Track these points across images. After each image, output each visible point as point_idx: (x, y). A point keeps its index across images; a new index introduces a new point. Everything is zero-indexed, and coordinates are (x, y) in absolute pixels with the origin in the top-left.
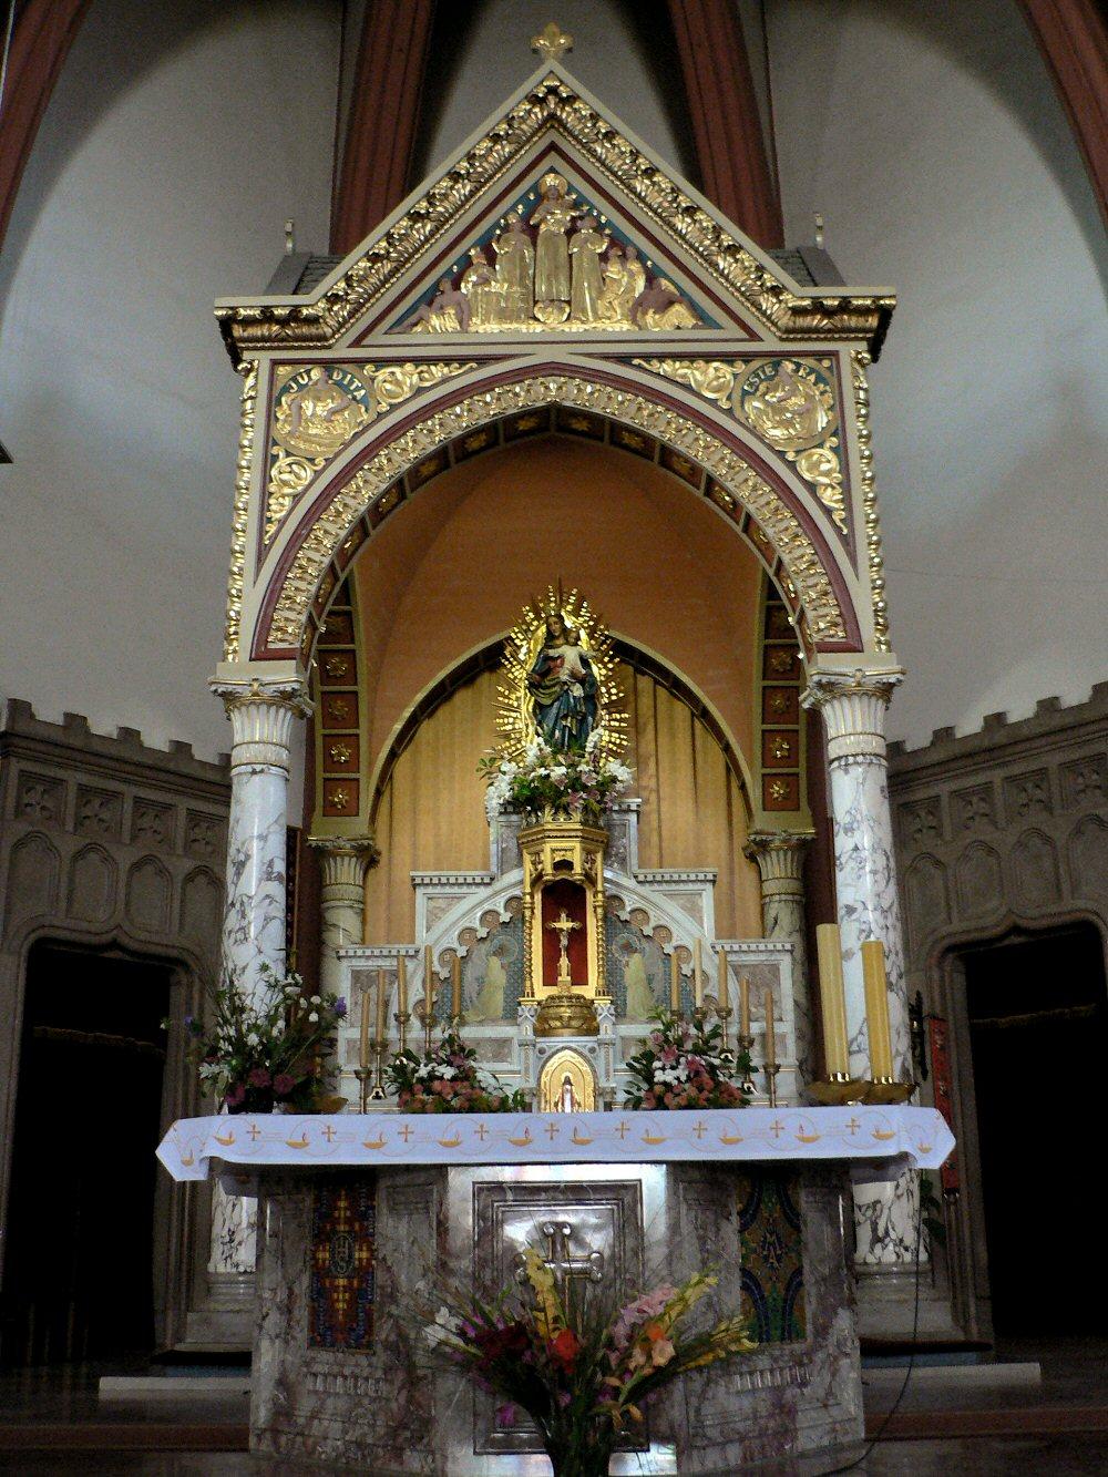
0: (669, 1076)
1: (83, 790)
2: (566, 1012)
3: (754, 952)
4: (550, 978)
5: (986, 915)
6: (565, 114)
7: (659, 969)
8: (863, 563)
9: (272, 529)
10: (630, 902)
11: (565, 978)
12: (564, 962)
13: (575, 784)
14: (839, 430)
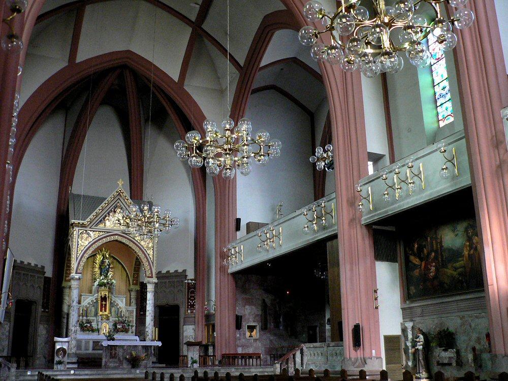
0: (119, 327)
1: (24, 274)
2: (105, 317)
3: (130, 308)
4: (101, 311)
5: (164, 302)
6: (121, 194)
7: (117, 310)
8: (154, 266)
9: (78, 255)
10: (113, 300)
11: (103, 311)
12: (103, 308)
13: (108, 283)
14: (153, 247)
